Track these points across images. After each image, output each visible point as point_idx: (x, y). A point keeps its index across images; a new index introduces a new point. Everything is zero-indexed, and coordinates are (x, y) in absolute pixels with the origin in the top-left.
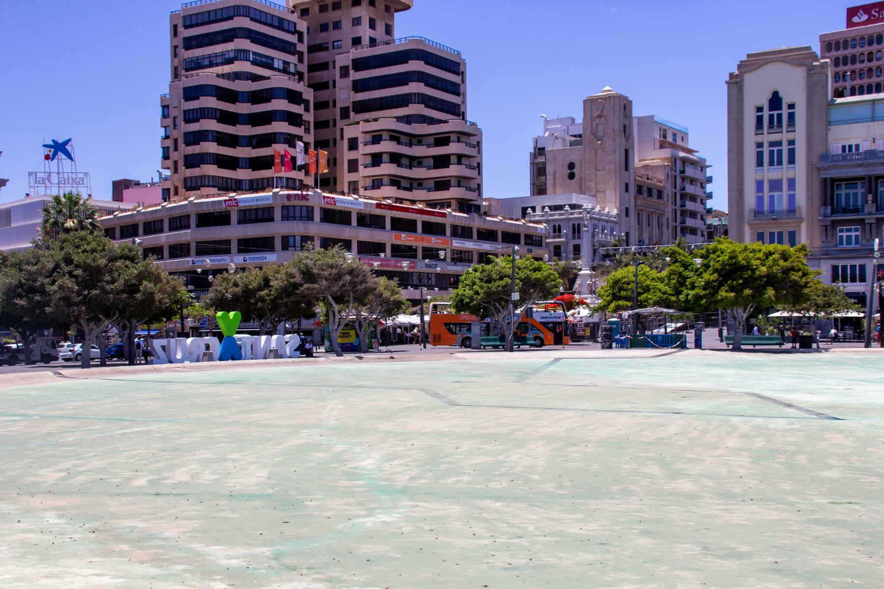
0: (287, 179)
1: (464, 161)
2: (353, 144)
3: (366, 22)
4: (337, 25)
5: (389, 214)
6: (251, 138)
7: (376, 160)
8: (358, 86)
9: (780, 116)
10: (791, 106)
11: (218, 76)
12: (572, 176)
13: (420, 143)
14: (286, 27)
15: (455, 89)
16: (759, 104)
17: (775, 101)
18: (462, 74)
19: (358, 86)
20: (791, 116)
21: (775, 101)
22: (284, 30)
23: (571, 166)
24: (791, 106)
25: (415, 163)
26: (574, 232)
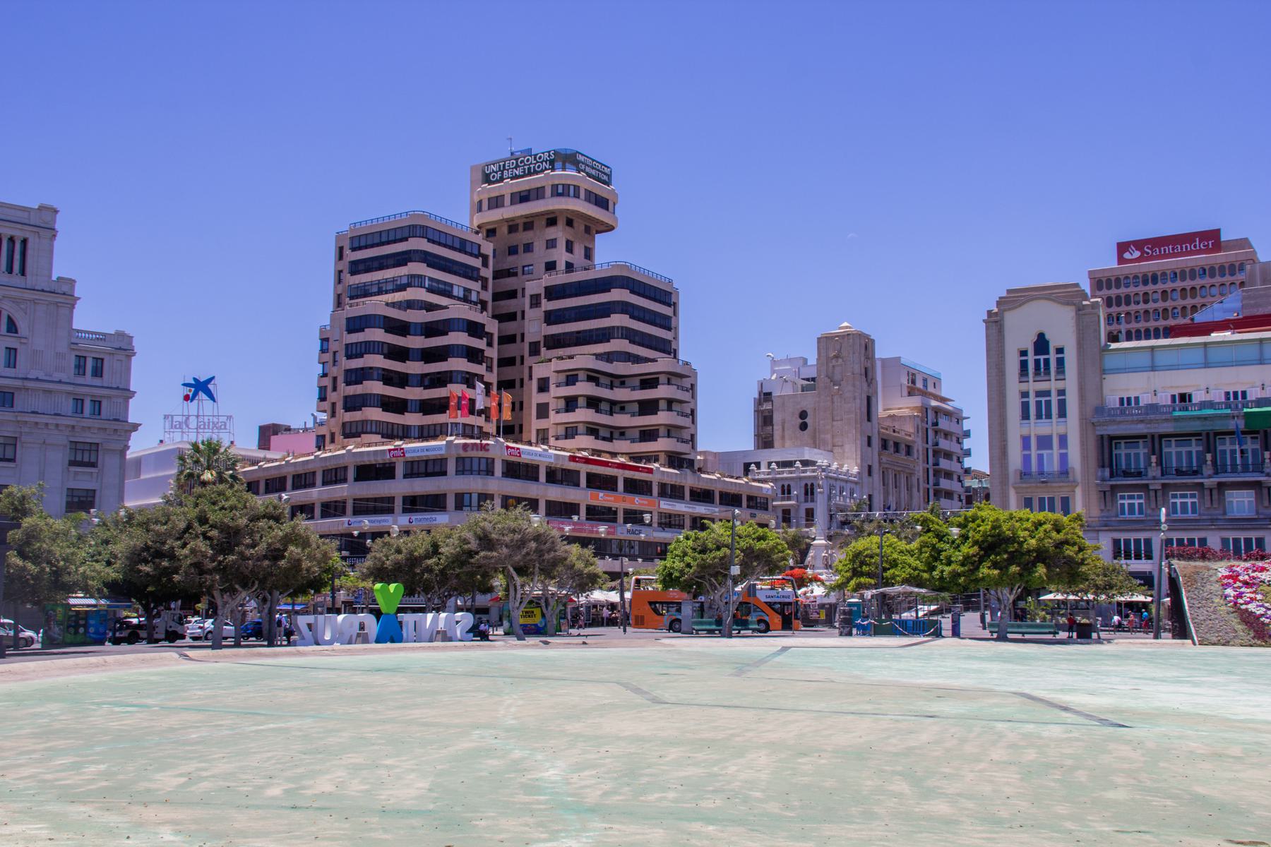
0: (464, 425)
1: (675, 406)
2: (543, 386)
3: (562, 245)
4: (528, 248)
5: (584, 469)
6: (424, 376)
7: (570, 404)
8: (551, 318)
9: (1047, 362)
10: (1060, 351)
11: (387, 304)
12: (804, 427)
13: (623, 384)
14: (468, 249)
15: (665, 323)
16: (1023, 347)
17: (1041, 344)
18: (674, 305)
19: (551, 318)
20: (1060, 362)
21: (1041, 344)
22: (466, 253)
23: (803, 415)
24: (1060, 351)
25: (617, 408)
26: (806, 494)
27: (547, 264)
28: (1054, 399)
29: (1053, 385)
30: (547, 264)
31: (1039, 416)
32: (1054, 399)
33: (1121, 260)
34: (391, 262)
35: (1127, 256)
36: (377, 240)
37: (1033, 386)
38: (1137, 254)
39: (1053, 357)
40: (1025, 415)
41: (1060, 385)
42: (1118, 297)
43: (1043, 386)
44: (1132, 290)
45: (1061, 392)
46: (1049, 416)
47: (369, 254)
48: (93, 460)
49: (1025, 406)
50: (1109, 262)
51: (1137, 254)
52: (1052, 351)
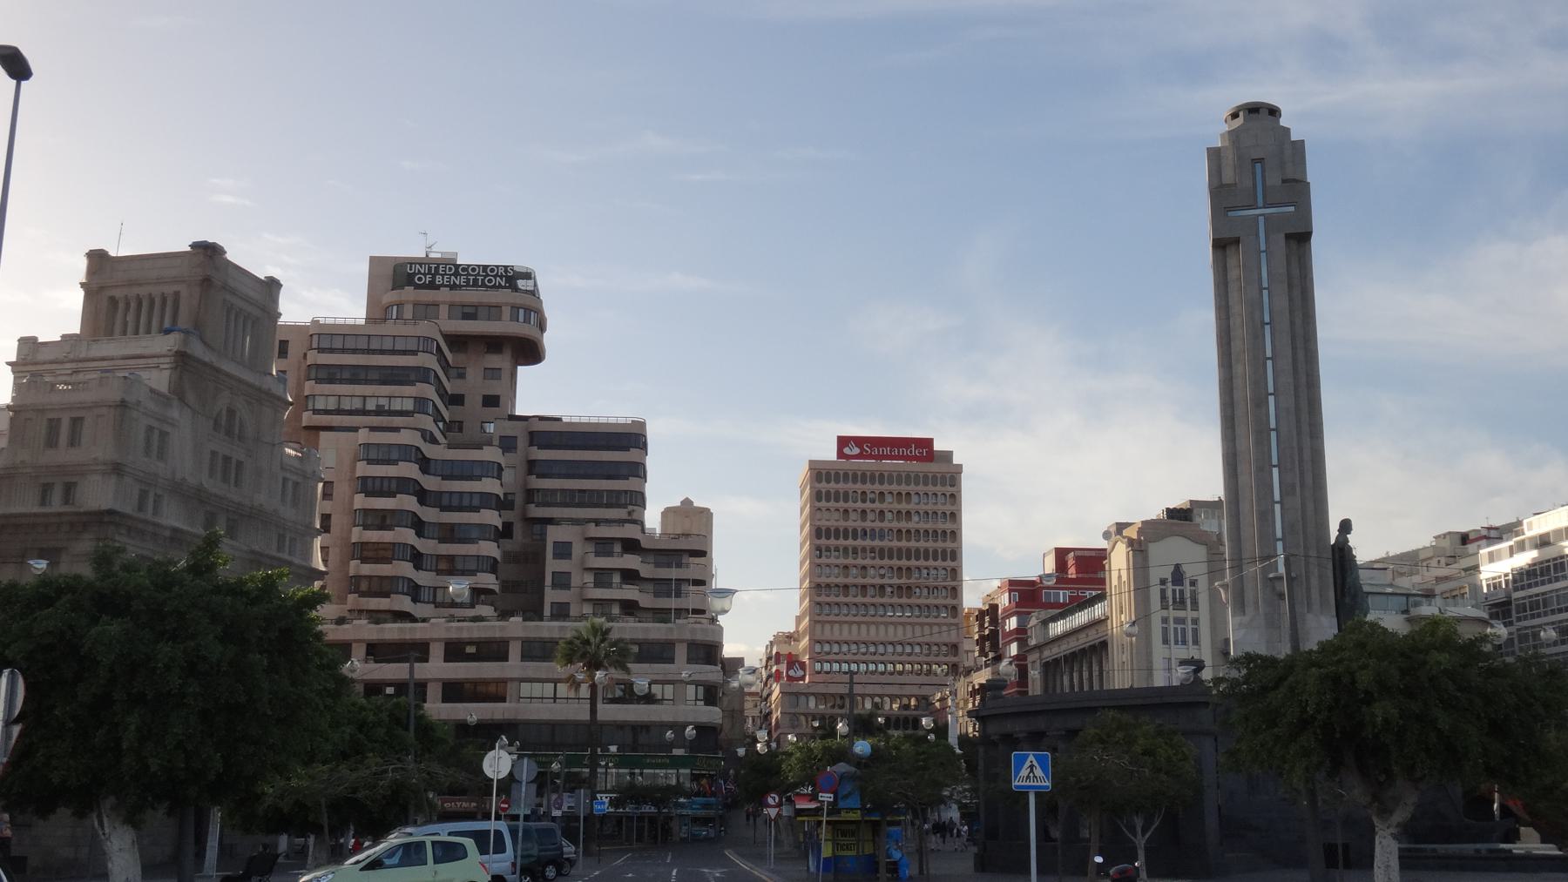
10: (1193, 583)
17: (1178, 576)
21: (1178, 576)
27: (485, 397)
28: (1190, 627)
29: (1189, 614)
30: (485, 397)
31: (1176, 643)
32: (1190, 627)
33: (840, 454)
34: (374, 376)
35: (847, 451)
36: (363, 345)
37: (1173, 613)
38: (856, 451)
39: (1188, 589)
40: (1166, 641)
41: (1195, 614)
42: (837, 493)
43: (1181, 614)
44: (850, 486)
45: (1195, 621)
46: (1184, 642)
47: (29, 345)
48: (819, 627)
49: (1165, 631)
50: (829, 453)
51: (856, 451)
52: (1187, 583)
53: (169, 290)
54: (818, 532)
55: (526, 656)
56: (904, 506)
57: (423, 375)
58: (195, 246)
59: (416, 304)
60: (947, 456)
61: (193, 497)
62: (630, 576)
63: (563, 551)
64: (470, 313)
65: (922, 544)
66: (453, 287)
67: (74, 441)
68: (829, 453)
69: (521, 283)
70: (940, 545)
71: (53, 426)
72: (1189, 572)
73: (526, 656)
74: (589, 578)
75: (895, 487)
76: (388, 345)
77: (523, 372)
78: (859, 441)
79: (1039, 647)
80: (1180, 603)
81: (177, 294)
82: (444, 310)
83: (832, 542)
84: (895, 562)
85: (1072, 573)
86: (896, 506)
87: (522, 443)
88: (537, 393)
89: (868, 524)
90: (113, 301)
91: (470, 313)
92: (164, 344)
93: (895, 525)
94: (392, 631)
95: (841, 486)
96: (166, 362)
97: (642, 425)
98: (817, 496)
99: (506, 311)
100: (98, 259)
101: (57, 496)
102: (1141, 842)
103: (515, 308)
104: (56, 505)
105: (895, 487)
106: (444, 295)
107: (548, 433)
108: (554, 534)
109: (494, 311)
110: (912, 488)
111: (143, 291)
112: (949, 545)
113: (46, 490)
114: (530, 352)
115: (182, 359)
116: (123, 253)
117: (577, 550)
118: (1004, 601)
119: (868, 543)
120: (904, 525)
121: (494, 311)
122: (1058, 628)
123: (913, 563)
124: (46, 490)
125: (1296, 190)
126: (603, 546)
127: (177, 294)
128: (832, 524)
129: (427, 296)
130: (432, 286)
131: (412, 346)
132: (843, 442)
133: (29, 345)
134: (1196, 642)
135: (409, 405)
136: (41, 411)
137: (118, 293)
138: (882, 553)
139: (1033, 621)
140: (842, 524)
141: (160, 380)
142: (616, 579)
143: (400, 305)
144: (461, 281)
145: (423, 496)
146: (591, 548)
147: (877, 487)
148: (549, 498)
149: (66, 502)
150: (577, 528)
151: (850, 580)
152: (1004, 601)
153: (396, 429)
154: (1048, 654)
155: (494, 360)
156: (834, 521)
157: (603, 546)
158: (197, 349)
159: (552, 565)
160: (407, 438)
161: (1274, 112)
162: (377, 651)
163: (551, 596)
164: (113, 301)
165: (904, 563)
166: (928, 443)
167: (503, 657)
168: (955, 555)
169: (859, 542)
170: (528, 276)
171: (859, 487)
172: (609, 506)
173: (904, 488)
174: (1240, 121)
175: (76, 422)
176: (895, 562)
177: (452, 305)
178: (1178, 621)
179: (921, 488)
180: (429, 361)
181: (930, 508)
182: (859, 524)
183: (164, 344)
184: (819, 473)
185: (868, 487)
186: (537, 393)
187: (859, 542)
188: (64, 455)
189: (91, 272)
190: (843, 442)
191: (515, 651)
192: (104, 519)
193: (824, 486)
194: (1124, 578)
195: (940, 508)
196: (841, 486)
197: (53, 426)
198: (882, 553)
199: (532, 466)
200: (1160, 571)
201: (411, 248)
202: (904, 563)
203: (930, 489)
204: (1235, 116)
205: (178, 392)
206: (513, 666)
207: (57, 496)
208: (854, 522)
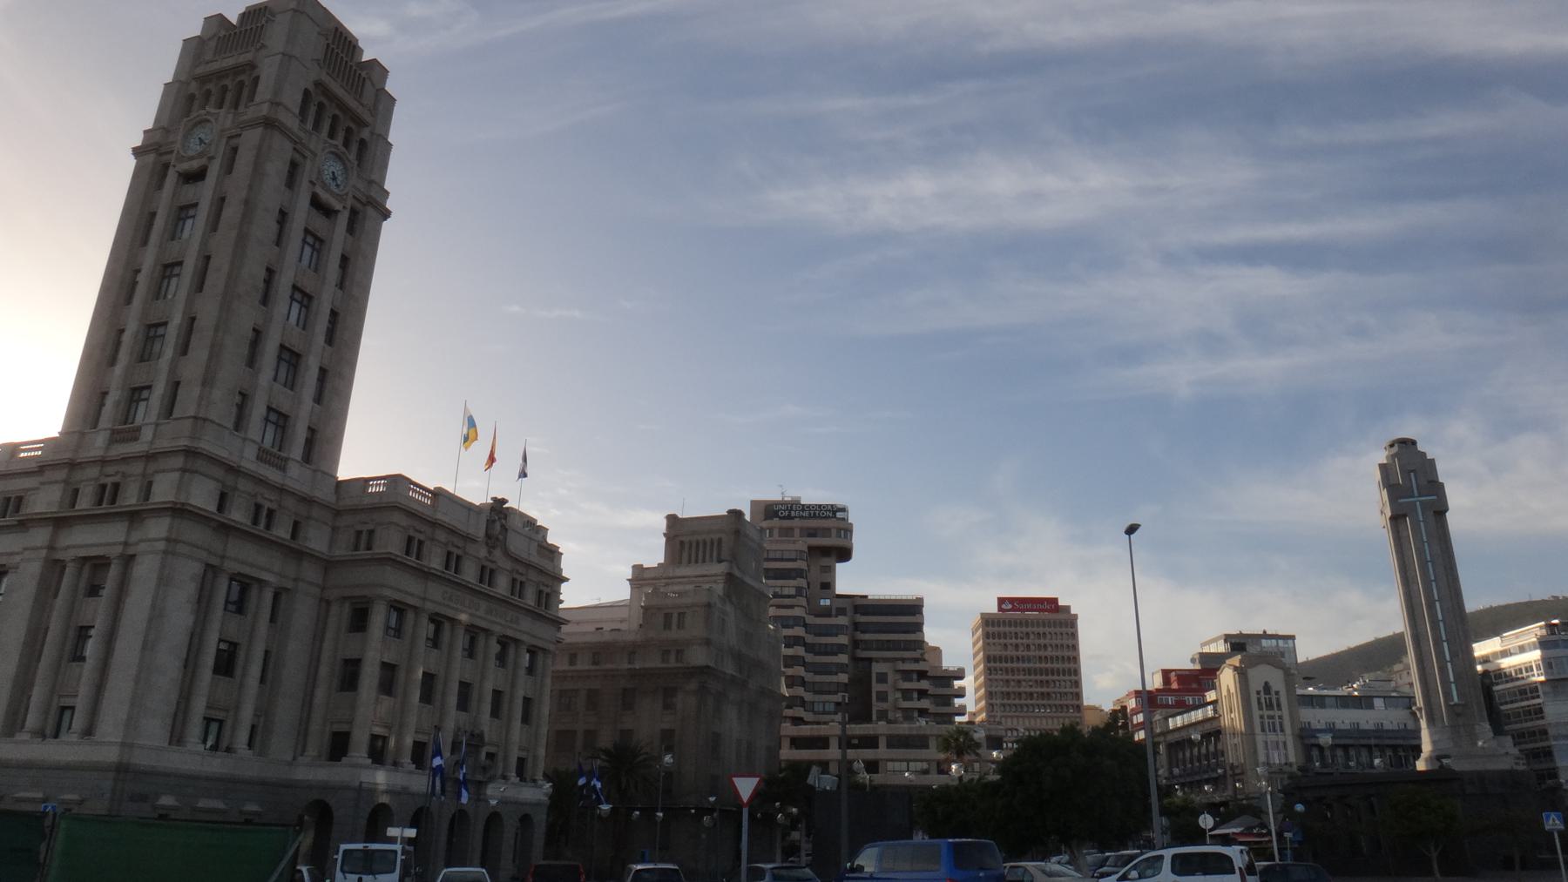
17: (1267, 688)
21: (1267, 688)
33: (1000, 609)
37: (1266, 713)
39: (1274, 697)
44: (1007, 629)
47: (638, 569)
50: (993, 608)
53: (716, 537)
54: (988, 659)
55: (889, 746)
56: (1042, 641)
57: (799, 573)
58: (730, 512)
59: (780, 528)
60: (1067, 609)
61: (738, 657)
62: (923, 694)
63: (882, 678)
64: (812, 533)
65: (1055, 665)
66: (802, 517)
67: (680, 626)
68: (993, 608)
69: (839, 515)
70: (1066, 665)
71: (668, 617)
72: (1274, 689)
73: (889, 746)
74: (899, 695)
75: (1035, 629)
76: (778, 555)
77: (840, 567)
78: (1012, 600)
79: (1162, 734)
80: (1270, 706)
81: (720, 540)
82: (797, 532)
83: (998, 665)
84: (1039, 677)
85: (1175, 686)
86: (1037, 642)
87: (850, 611)
88: (849, 580)
89: (1020, 653)
90: (682, 543)
91: (812, 533)
92: (721, 568)
93: (1037, 653)
94: (805, 730)
95: (1002, 629)
96: (721, 579)
97: (921, 600)
98: (987, 636)
99: (834, 532)
100: (672, 520)
101: (672, 658)
102: (1435, 855)
103: (839, 530)
104: (672, 663)
105: (1035, 629)
106: (797, 523)
107: (860, 606)
108: (877, 668)
109: (826, 532)
110: (1047, 630)
111: (700, 538)
112: (1072, 665)
113: (666, 653)
114: (845, 554)
115: (729, 577)
116: (685, 516)
117: (890, 678)
118: (1132, 704)
119: (1021, 665)
120: (1042, 653)
121: (826, 532)
122: (1178, 721)
123: (1050, 677)
124: (666, 653)
125: (1436, 489)
126: (906, 675)
127: (720, 540)
128: (998, 653)
129: (786, 523)
130: (789, 517)
131: (793, 556)
132: (1001, 601)
133: (638, 569)
134: (1282, 730)
135: (793, 592)
136: (659, 609)
137: (686, 539)
138: (1029, 671)
139: (1157, 717)
140: (1004, 653)
141: (719, 588)
142: (915, 695)
143: (771, 529)
144: (806, 514)
145: (810, 648)
146: (898, 676)
147: (1024, 629)
148: (868, 645)
149: (677, 660)
150: (889, 664)
151: (1010, 689)
152: (1132, 704)
153: (792, 607)
154: (1170, 738)
155: (825, 561)
156: (997, 652)
157: (906, 675)
158: (737, 573)
159: (876, 687)
160: (798, 612)
161: (1414, 443)
162: (797, 743)
163: (877, 706)
164: (682, 543)
165: (1044, 677)
166: (1055, 601)
167: (926, 746)
168: (1077, 672)
169: (1015, 665)
170: (843, 510)
171: (1013, 629)
172: (906, 649)
173: (1041, 630)
174: (1395, 449)
175: (681, 615)
176: (1039, 677)
177: (801, 529)
178: (1270, 717)
179: (1052, 630)
180: (801, 565)
181: (1059, 642)
182: (1014, 653)
183: (721, 568)
184: (987, 620)
185: (1019, 629)
186: (849, 580)
187: (1015, 665)
188: (674, 634)
189: (669, 527)
190: (1001, 601)
191: (882, 742)
192: (704, 670)
193: (990, 629)
194: (1233, 690)
195: (1065, 642)
196: (1002, 629)
197: (668, 617)
198: (1029, 671)
199: (856, 626)
200: (1256, 685)
201: (775, 496)
202: (1044, 677)
203: (1058, 630)
204: (1392, 446)
205: (727, 596)
206: (882, 752)
207: (672, 658)
208: (1011, 652)
